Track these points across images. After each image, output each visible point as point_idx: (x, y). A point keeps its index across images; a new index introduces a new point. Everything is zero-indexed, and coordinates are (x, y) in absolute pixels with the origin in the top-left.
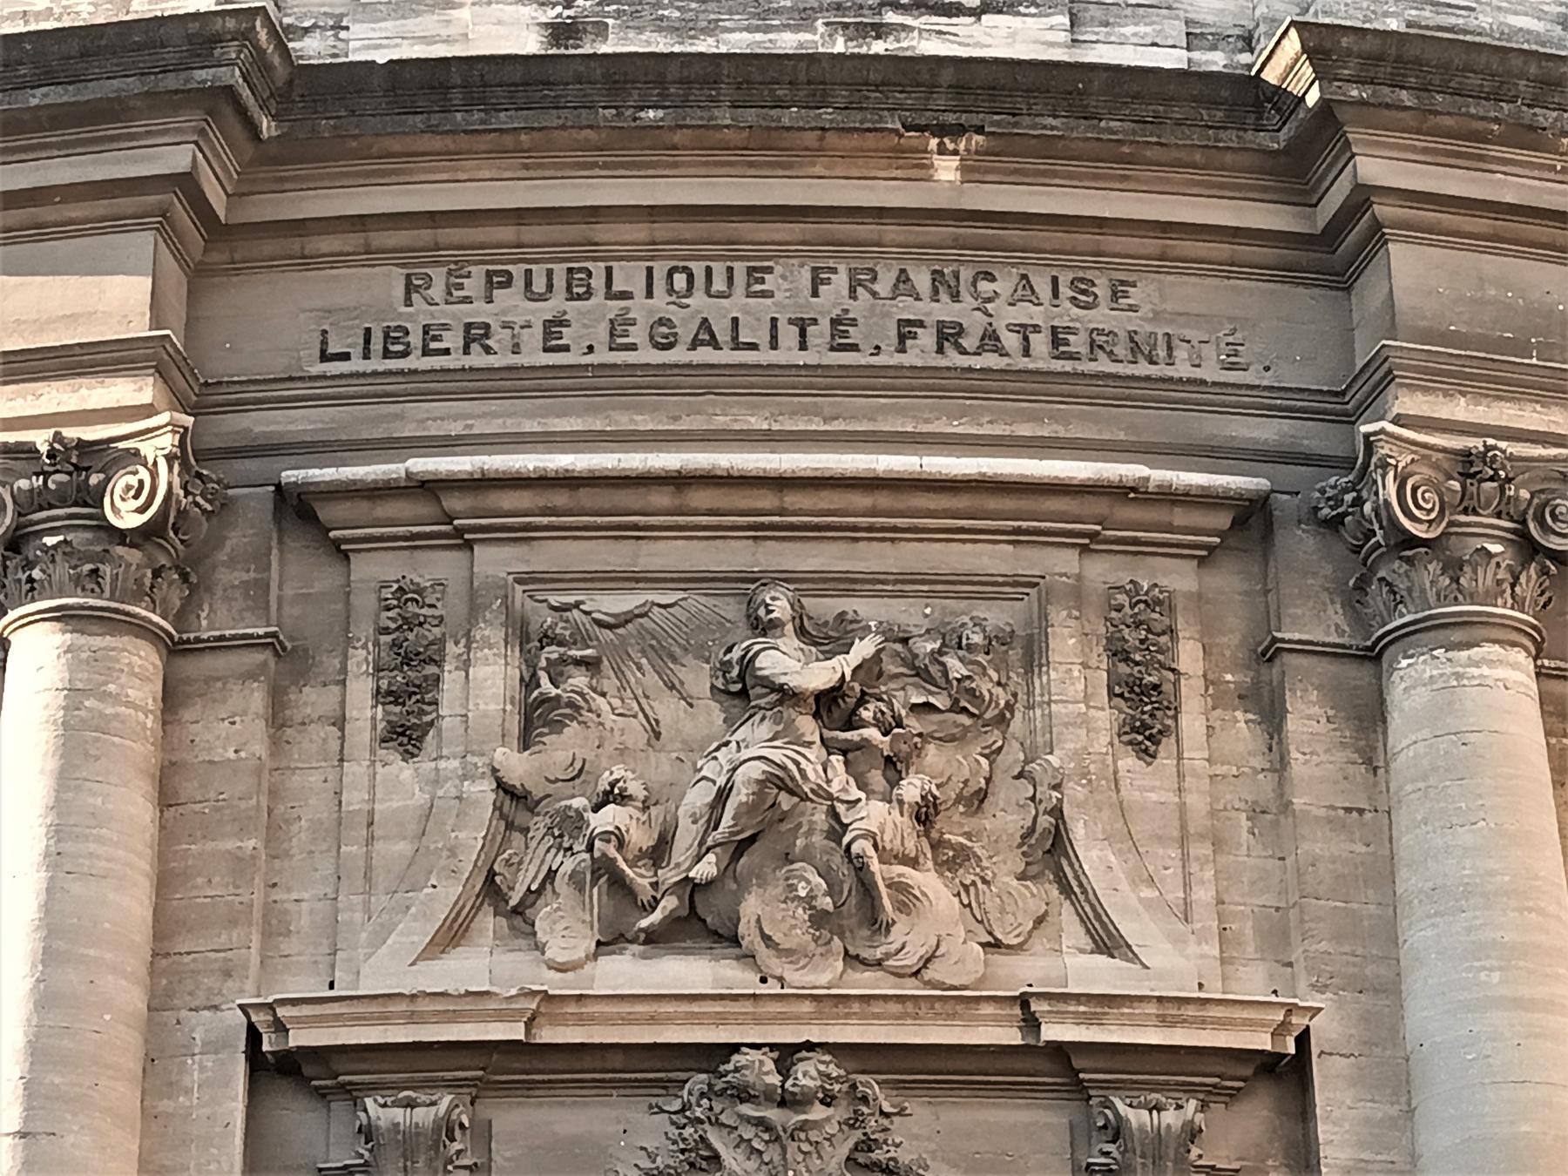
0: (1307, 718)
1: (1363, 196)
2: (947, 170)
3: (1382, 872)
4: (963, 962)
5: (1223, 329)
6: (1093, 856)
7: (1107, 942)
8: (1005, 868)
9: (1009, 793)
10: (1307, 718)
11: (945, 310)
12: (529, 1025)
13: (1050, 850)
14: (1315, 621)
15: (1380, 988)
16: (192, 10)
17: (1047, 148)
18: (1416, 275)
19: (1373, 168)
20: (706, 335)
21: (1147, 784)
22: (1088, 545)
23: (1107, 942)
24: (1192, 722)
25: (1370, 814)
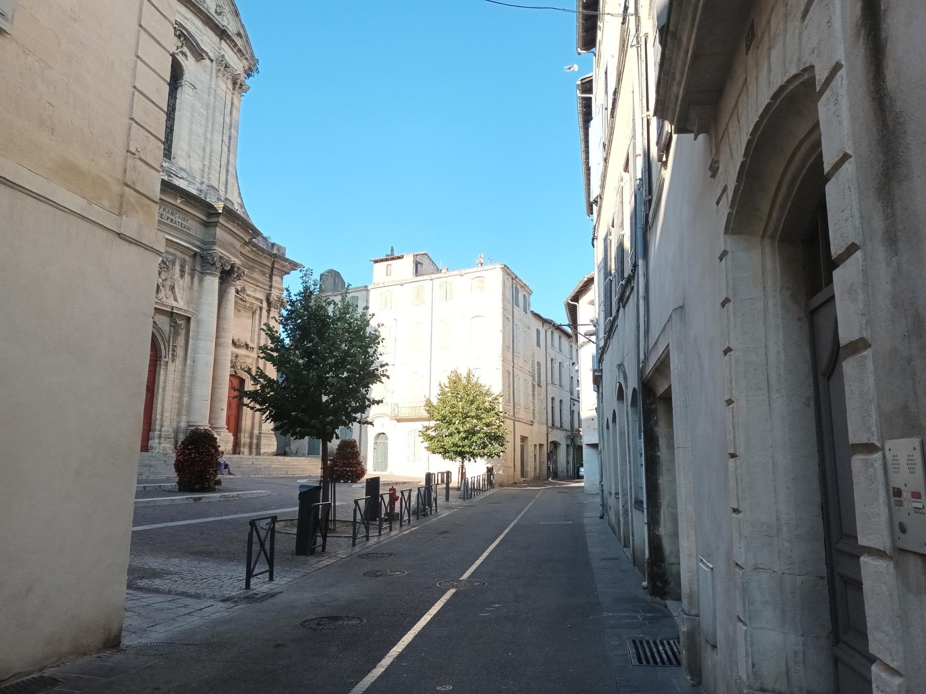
0: (196, 279)
1: (218, 222)
2: (179, 201)
3: (200, 298)
4: (164, 300)
5: (195, 229)
6: (177, 290)
7: (176, 300)
8: (168, 288)
9: (170, 280)
10: (196, 279)
11: (171, 217)
12: (594, 446)
13: (172, 288)
14: (198, 268)
15: (197, 311)
16: (501, 334)
17: (190, 203)
18: (219, 233)
19: (221, 220)
20: (172, 220)
21: (181, 282)
22: (181, 252)
23: (176, 300)
24: (186, 276)
25: (200, 291)
